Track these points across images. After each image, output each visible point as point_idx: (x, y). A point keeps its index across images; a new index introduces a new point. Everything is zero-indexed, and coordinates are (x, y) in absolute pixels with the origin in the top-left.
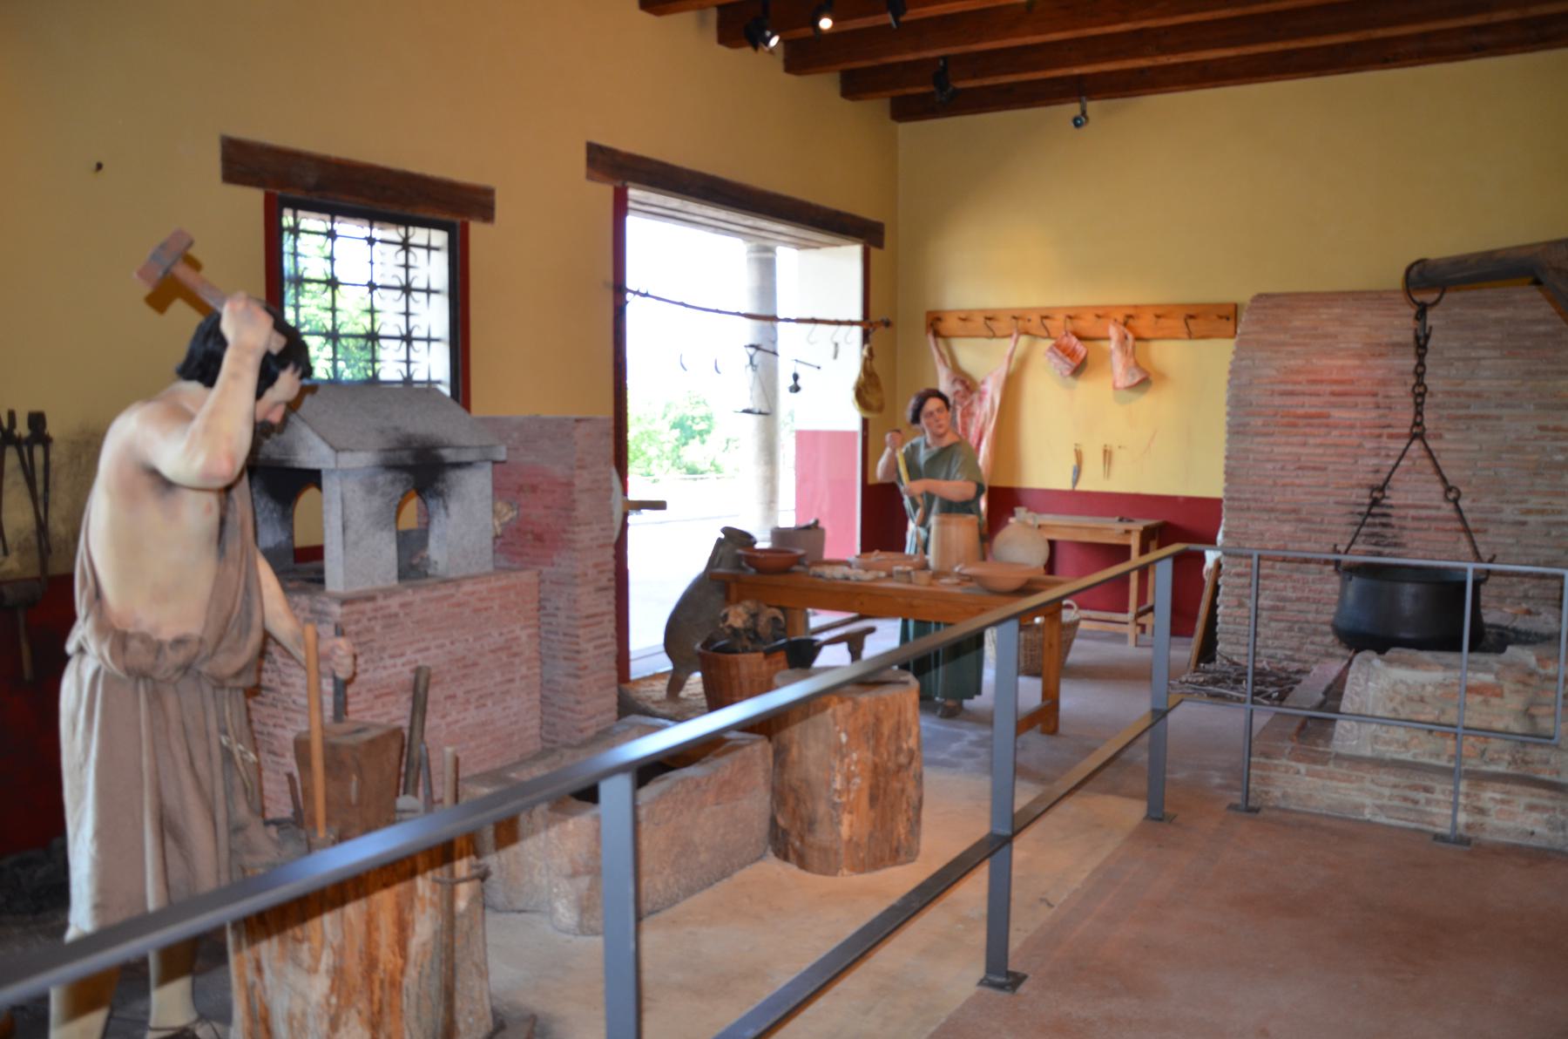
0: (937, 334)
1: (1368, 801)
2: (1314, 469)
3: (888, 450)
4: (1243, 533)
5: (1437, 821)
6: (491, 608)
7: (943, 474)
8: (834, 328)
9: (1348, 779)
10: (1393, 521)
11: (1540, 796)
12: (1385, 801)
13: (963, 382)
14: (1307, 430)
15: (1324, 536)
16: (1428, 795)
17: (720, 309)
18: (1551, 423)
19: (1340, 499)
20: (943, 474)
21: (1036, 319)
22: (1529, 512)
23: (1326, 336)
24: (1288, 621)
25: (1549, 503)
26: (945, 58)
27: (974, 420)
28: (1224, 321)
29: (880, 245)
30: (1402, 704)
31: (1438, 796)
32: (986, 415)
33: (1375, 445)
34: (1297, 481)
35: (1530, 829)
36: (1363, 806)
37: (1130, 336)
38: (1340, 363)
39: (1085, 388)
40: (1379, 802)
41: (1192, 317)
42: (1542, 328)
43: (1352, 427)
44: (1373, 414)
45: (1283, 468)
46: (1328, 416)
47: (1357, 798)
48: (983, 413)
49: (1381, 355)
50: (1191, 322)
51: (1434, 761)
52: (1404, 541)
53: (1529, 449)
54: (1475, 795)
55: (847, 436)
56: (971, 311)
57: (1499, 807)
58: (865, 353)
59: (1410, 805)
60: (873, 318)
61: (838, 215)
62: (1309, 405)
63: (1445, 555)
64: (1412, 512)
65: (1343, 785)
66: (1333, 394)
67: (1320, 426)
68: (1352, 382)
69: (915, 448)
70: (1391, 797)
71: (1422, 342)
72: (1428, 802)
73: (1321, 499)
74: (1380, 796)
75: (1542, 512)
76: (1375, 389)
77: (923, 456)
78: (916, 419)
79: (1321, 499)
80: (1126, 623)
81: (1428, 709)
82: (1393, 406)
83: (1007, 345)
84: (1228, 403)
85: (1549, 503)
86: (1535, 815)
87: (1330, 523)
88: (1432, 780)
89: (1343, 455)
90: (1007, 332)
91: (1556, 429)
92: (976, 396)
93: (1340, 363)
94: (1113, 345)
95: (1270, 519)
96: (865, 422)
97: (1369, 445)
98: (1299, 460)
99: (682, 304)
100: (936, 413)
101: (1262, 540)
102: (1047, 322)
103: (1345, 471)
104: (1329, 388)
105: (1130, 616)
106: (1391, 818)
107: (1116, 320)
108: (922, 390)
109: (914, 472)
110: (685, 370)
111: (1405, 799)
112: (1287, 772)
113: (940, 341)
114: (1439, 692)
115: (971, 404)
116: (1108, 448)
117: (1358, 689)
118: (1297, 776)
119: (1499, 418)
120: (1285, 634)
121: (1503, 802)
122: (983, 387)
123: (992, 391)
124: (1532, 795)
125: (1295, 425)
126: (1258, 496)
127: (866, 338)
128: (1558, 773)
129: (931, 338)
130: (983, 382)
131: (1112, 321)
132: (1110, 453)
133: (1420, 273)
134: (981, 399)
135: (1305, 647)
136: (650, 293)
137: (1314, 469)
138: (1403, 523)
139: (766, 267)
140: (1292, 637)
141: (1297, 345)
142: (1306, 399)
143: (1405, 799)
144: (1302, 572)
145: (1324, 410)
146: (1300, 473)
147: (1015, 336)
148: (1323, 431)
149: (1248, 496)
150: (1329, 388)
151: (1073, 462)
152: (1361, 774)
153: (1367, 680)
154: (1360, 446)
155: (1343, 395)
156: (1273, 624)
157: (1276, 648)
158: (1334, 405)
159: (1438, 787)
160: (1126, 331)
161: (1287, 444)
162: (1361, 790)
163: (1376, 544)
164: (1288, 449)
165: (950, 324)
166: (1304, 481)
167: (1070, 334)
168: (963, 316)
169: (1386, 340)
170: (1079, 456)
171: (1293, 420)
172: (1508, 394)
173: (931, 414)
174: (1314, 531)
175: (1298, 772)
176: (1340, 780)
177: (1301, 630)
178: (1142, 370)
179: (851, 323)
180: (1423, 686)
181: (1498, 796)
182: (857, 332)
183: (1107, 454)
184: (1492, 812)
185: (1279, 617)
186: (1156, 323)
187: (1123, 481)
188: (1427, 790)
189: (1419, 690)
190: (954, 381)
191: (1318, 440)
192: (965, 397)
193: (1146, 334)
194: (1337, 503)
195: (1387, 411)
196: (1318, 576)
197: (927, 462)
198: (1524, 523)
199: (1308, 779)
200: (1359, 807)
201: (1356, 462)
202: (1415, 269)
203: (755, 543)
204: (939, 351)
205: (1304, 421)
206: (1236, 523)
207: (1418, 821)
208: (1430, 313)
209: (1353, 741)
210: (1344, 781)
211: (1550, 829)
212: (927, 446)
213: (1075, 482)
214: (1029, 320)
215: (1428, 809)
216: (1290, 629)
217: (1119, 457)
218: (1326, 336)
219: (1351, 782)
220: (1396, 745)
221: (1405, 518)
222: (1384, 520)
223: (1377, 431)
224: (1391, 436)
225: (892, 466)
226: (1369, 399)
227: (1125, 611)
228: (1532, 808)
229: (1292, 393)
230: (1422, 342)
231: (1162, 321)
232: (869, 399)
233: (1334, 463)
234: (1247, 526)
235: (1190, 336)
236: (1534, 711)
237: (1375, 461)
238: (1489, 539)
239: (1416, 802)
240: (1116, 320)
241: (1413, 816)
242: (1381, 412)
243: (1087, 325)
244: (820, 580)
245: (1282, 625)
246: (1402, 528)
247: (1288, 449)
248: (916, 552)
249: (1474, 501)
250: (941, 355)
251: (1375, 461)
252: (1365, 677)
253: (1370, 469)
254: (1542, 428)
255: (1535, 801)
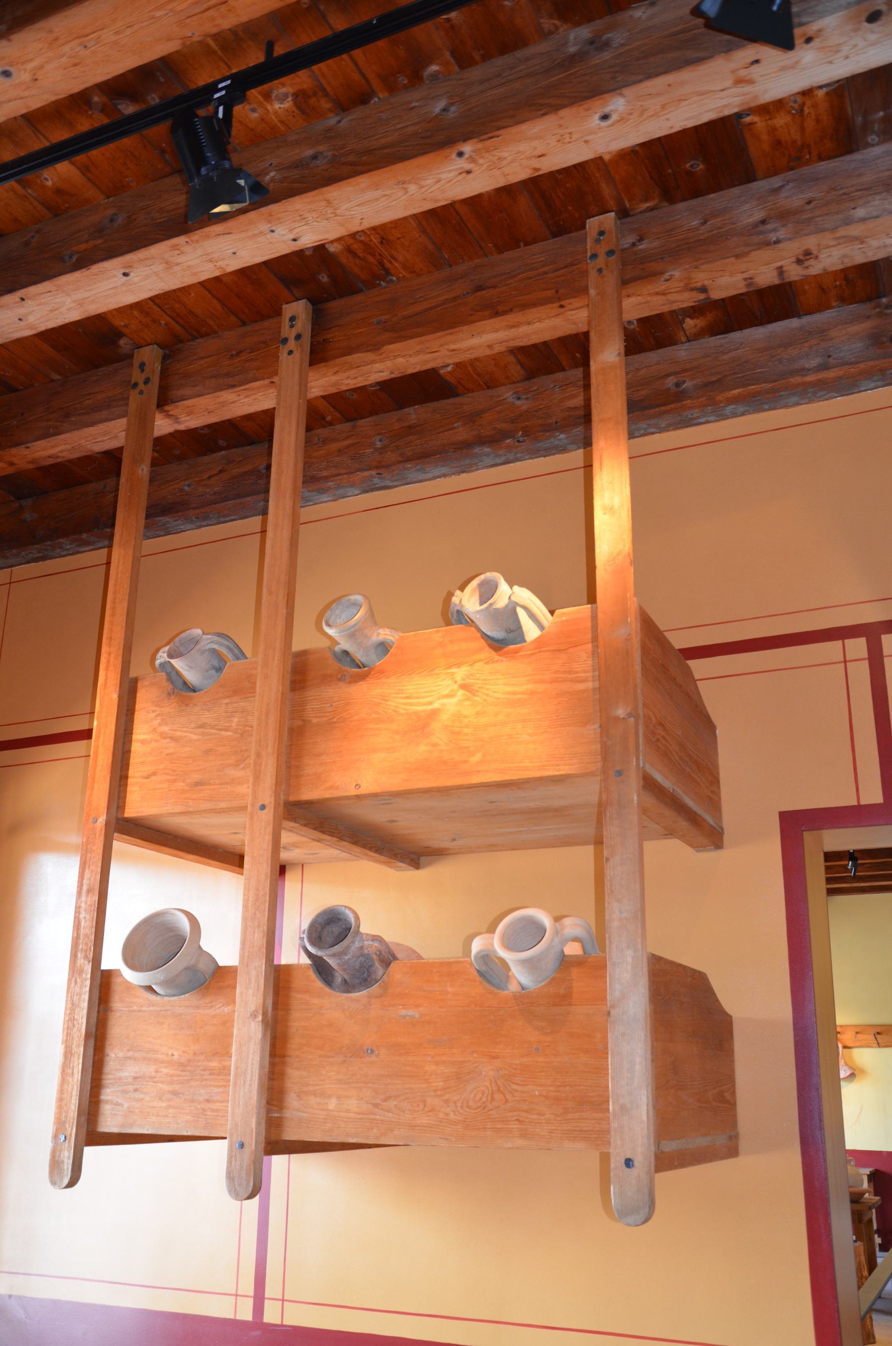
6: (122, 1105)
41: (878, 1033)
50: (878, 1037)
63: (866, 865)
139: (50, 142)
178: (851, 1068)
179: (236, 1299)
186: (856, 1037)
193: (849, 1045)
231: (858, 1035)
235: (879, 1045)
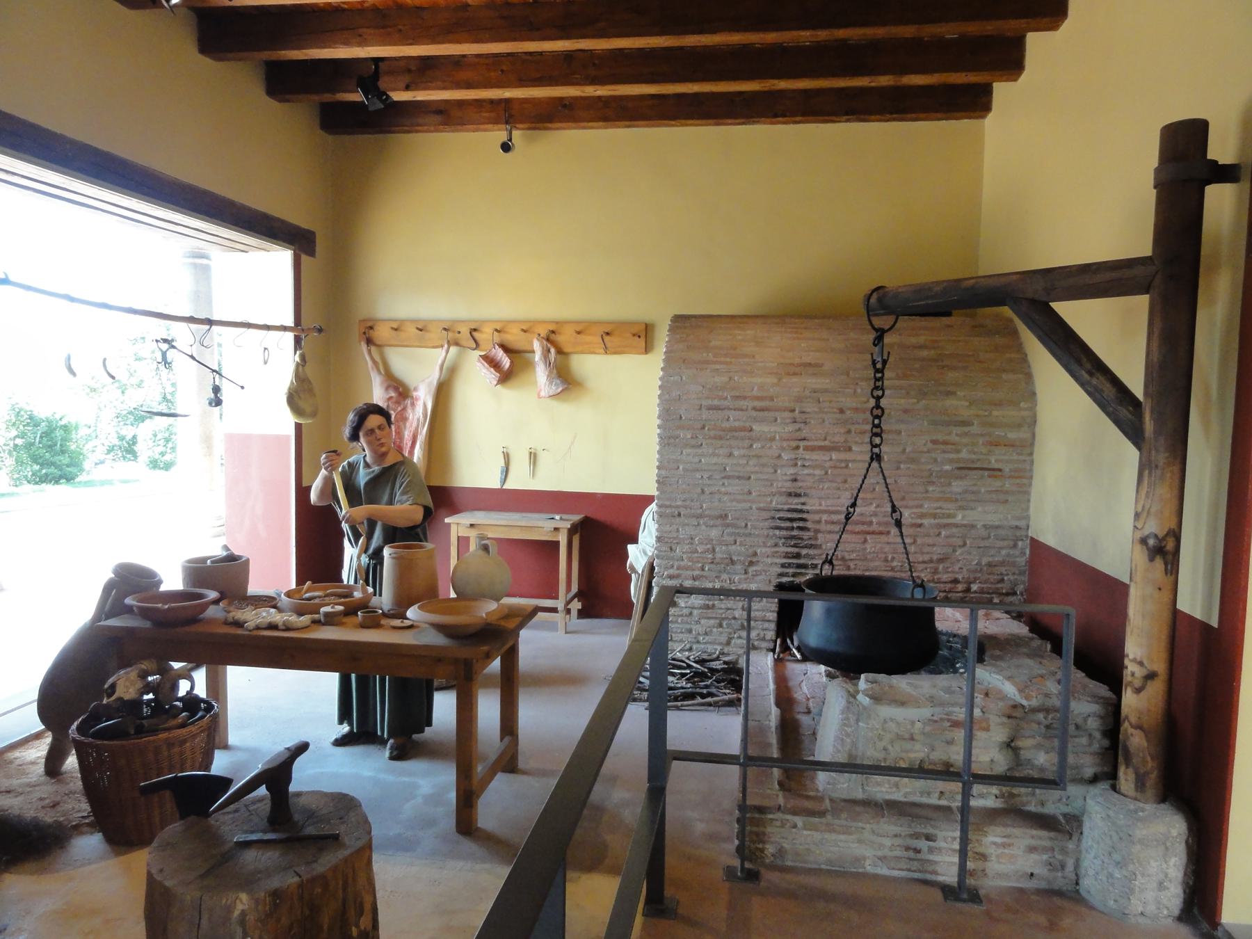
0: (369, 341)
1: (869, 853)
2: (739, 478)
3: (323, 472)
4: (674, 538)
5: (939, 870)
7: (386, 498)
8: (264, 332)
9: (847, 832)
10: (809, 525)
11: (1040, 838)
12: (887, 852)
13: (396, 389)
14: (733, 443)
15: (748, 539)
16: (931, 843)
17: (73, 295)
18: (940, 437)
19: (762, 505)
20: (386, 498)
21: (465, 330)
22: (922, 516)
23: (745, 356)
24: (716, 618)
25: (940, 508)
26: (377, 61)
27: (408, 424)
28: (637, 338)
29: (312, 253)
30: (892, 742)
31: (941, 844)
32: (418, 420)
33: (793, 456)
34: (723, 489)
35: (1029, 871)
36: (864, 858)
37: (553, 350)
38: (760, 380)
39: (510, 395)
40: (880, 853)
41: (608, 334)
42: (925, 353)
43: (773, 439)
44: (791, 428)
45: (709, 478)
46: (751, 430)
47: (857, 850)
48: (416, 417)
49: (795, 374)
50: (607, 338)
51: (925, 800)
52: (819, 542)
53: (923, 460)
54: (977, 840)
55: (280, 440)
56: (402, 322)
57: (1000, 851)
58: (297, 359)
59: (911, 854)
60: (305, 323)
61: (266, 217)
62: (735, 419)
64: (825, 517)
65: (842, 837)
66: (754, 409)
67: (743, 439)
68: (772, 399)
69: (352, 467)
70: (892, 848)
71: (879, 366)
72: (931, 850)
73: (747, 505)
74: (881, 846)
75: (935, 516)
76: (792, 405)
77: (362, 477)
78: (354, 437)
79: (747, 505)
80: (554, 610)
81: (918, 746)
82: (808, 421)
83: (441, 353)
84: (659, 417)
85: (940, 508)
86: (1034, 857)
87: (754, 527)
88: (933, 827)
89: (764, 465)
90: (440, 343)
91: (945, 443)
92: (409, 402)
93: (760, 380)
94: (538, 356)
95: (698, 524)
96: (298, 427)
97: (785, 456)
98: (725, 469)
99: (72, 299)
100: (377, 431)
101: (692, 544)
102: (475, 334)
103: (767, 480)
104: (751, 404)
105: (559, 604)
106: (893, 869)
107: (539, 335)
108: (360, 404)
109: (354, 497)
110: (74, 374)
111: (907, 849)
112: (782, 826)
113: (373, 348)
114: (928, 729)
115: (404, 409)
116: (532, 451)
117: (849, 730)
118: (794, 830)
119: (899, 433)
120: (715, 630)
121: (1004, 845)
122: (415, 394)
123: (424, 397)
124: (1033, 837)
125: (721, 438)
126: (688, 503)
127: (298, 341)
128: (1043, 804)
129: (364, 347)
130: (416, 389)
131: (537, 336)
132: (535, 455)
133: (880, 300)
134: (413, 405)
135: (733, 641)
136: (12, 278)
137: (739, 478)
138: (818, 527)
140: (721, 633)
141: (721, 363)
142: (732, 414)
143: (907, 849)
144: (728, 573)
145: (747, 425)
146: (726, 482)
147: (446, 346)
148: (747, 443)
149: (679, 503)
150: (751, 404)
151: (502, 463)
152: (860, 824)
153: (858, 721)
154: (779, 457)
155: (765, 408)
156: (703, 621)
157: (705, 643)
158: (755, 420)
159: (940, 834)
160: (549, 345)
161: (714, 455)
162: (860, 841)
163: (795, 546)
164: (715, 460)
165: (382, 333)
166: (730, 489)
167: (497, 347)
168: (395, 326)
169: (797, 361)
170: (507, 457)
171: (721, 433)
172: (906, 411)
173: (372, 431)
174: (738, 534)
175: (795, 826)
176: (839, 833)
177: (729, 625)
179: (284, 328)
180: (913, 723)
181: (999, 840)
182: (289, 337)
183: (533, 457)
184: (993, 858)
185: (710, 615)
187: (546, 481)
188: (929, 838)
189: (909, 727)
190: (387, 388)
191: (742, 452)
192: (398, 403)
194: (759, 509)
195: (802, 425)
196: (743, 576)
197: (367, 484)
198: (920, 525)
199: (805, 832)
200: (858, 860)
201: (776, 471)
202: (875, 296)
203: (160, 582)
204: (372, 358)
205: (730, 434)
206: (668, 528)
207: (920, 871)
208: (888, 339)
209: (843, 784)
210: (844, 833)
211: (1049, 870)
212: (367, 465)
213: (504, 481)
214: (459, 332)
215: (931, 857)
216: (721, 625)
217: (543, 459)
218: (745, 356)
219: (850, 834)
220: (887, 786)
221: (819, 522)
222: (801, 524)
223: (794, 444)
224: (806, 448)
225: (329, 488)
226: (787, 414)
227: (556, 598)
228: (1032, 849)
229: (717, 408)
230: (879, 366)
232: (302, 404)
233: (757, 472)
234: (678, 531)
235: (606, 350)
236: (1020, 743)
237: (792, 471)
238: (891, 540)
239: (917, 851)
240: (539, 335)
241: (915, 865)
242: (797, 426)
243: (514, 337)
244: (240, 632)
245: (712, 622)
246: (817, 531)
247: (715, 460)
248: (356, 582)
249: (878, 506)
250: (374, 362)
251: (792, 471)
252: (855, 718)
253: (788, 478)
254: (934, 442)
255: (1033, 842)
